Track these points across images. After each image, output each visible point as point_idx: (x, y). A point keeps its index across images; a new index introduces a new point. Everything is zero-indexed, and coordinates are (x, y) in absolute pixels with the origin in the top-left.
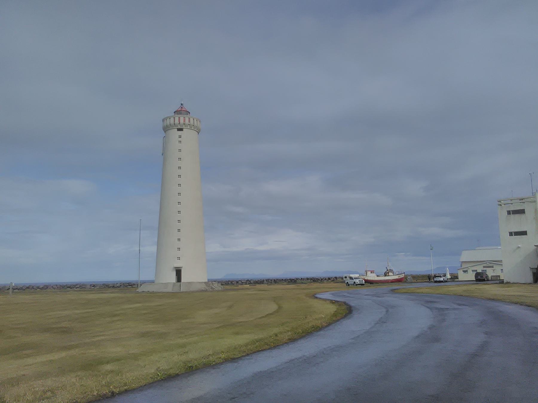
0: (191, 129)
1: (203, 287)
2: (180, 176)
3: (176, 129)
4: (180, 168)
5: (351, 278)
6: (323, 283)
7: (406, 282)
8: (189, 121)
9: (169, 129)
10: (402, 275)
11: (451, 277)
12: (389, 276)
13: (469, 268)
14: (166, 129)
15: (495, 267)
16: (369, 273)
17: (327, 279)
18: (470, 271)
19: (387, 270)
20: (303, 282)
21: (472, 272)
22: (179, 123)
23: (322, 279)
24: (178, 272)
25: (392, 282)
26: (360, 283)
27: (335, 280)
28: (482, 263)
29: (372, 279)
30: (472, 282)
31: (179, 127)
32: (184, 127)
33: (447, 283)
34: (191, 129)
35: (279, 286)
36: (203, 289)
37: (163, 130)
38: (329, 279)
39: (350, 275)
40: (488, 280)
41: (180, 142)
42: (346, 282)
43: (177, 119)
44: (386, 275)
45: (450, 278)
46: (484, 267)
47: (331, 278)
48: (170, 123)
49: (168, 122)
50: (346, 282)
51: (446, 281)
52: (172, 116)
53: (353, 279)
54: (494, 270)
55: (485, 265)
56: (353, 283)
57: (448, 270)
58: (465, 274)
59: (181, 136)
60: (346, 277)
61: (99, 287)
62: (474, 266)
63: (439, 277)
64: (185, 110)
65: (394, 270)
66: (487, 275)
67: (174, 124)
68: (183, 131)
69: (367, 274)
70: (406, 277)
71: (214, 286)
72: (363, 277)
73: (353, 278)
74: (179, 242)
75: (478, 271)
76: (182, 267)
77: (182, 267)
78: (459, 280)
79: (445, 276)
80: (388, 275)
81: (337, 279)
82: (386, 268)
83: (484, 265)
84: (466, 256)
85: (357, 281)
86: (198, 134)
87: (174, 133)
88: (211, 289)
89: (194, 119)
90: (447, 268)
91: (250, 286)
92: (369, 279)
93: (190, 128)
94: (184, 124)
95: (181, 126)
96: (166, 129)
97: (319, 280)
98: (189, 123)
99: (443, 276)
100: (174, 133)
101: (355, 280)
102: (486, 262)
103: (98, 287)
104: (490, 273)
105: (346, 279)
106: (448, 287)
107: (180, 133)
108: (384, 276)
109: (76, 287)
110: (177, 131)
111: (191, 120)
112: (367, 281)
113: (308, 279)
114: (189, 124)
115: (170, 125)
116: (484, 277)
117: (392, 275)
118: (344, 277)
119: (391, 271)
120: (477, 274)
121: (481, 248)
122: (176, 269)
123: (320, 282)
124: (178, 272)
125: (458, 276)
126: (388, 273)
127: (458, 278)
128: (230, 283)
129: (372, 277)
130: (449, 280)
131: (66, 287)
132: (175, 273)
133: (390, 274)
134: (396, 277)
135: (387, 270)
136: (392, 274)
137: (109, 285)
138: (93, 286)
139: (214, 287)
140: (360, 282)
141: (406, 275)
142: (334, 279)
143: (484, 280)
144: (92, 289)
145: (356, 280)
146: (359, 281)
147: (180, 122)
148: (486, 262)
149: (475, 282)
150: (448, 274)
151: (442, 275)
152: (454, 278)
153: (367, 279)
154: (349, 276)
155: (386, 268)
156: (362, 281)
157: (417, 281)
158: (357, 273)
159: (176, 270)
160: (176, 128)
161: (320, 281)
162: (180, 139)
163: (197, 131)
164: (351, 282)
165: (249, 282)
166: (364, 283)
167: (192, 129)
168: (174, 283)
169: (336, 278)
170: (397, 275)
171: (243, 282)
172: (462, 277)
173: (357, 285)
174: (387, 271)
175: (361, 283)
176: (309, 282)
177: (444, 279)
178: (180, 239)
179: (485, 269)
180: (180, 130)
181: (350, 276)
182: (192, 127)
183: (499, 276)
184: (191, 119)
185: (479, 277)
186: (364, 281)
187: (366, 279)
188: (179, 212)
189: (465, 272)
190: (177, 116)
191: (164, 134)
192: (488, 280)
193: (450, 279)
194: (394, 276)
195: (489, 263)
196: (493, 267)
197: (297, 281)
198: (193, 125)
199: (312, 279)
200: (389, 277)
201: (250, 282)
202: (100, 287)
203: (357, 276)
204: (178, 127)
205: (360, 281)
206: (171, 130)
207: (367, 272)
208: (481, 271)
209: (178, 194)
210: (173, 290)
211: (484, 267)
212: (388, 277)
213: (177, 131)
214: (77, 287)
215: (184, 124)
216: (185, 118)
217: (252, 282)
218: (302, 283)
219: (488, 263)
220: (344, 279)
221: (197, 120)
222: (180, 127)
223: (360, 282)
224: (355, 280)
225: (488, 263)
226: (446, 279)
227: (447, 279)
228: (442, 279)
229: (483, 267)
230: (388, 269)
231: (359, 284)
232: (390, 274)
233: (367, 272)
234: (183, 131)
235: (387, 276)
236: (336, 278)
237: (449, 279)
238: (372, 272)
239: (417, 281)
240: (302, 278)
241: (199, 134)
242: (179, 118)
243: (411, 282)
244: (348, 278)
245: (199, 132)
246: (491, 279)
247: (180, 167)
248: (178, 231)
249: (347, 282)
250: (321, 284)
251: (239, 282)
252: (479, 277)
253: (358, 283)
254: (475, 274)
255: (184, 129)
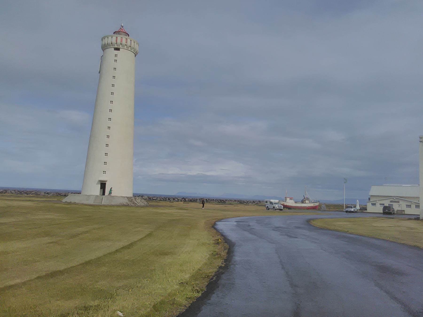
0: (128, 50)
1: (125, 201)
2: (112, 93)
3: (113, 48)
4: (113, 86)
5: (271, 203)
6: (248, 205)
7: (319, 210)
8: (126, 42)
9: (106, 48)
10: (317, 203)
11: (360, 208)
12: (305, 203)
13: (377, 202)
14: (104, 47)
15: (401, 202)
16: (288, 199)
17: (252, 202)
18: (378, 205)
19: (304, 198)
20: (231, 203)
21: (379, 205)
22: (116, 43)
23: (247, 202)
24: (103, 185)
25: (308, 209)
26: (278, 208)
27: (258, 203)
28: (388, 198)
29: (290, 205)
30: (378, 215)
31: (116, 47)
32: (121, 47)
33: (356, 214)
34: (128, 50)
35: (210, 205)
36: (125, 204)
37: (102, 48)
38: (254, 202)
39: (270, 200)
40: (394, 214)
41: (116, 61)
42: (267, 206)
43: (114, 38)
44: (303, 202)
45: (360, 209)
46: (391, 202)
47: (256, 201)
48: (107, 42)
49: (106, 41)
50: (267, 206)
51: (356, 212)
52: (110, 36)
53: (273, 204)
54: (400, 205)
55: (391, 200)
56: (273, 207)
57: (358, 202)
58: (373, 207)
59: (115, 56)
60: (266, 202)
61: (52, 195)
62: (382, 200)
63: (350, 208)
64: (125, 32)
65: (310, 199)
66: (393, 209)
67: (112, 43)
68: (119, 50)
69: (287, 200)
70: (320, 206)
71: (136, 202)
72: (282, 203)
73: (273, 202)
74: (106, 156)
75: (385, 205)
76: (107, 181)
77: (107, 181)
78: (368, 212)
79: (355, 207)
80: (304, 202)
81: (260, 202)
82: (304, 196)
83: (391, 200)
84: (375, 191)
85: (277, 206)
86: (135, 56)
87: (111, 52)
88: (133, 203)
89: (131, 40)
90: (358, 200)
91: (183, 203)
92: (288, 204)
93: (127, 49)
94: (121, 44)
95: (117, 46)
96: (104, 47)
97: (245, 202)
98: (126, 44)
99: (354, 207)
100: (111, 52)
101: (274, 205)
102: (393, 197)
103: (51, 195)
104: (396, 207)
105: (266, 203)
106: (373, 217)
107: (116, 52)
108: (301, 203)
109: (32, 193)
110: (114, 50)
111: (129, 41)
112: (285, 207)
113: (235, 201)
114: (126, 45)
115: (107, 44)
116: (391, 211)
117: (308, 203)
118: (265, 201)
119: (308, 199)
120: (385, 208)
121: (388, 185)
122: (101, 182)
123: (245, 204)
124: (103, 185)
125: (367, 207)
126: (305, 201)
127: (367, 210)
128: (167, 199)
129: (290, 203)
130: (358, 211)
131: (23, 193)
132: (99, 186)
133: (307, 201)
134: (312, 205)
135: (304, 198)
136: (309, 202)
137: (61, 194)
138: (47, 194)
139: (136, 203)
140: (279, 207)
141: (320, 204)
142: (258, 202)
143: (390, 214)
144: (46, 196)
145: (276, 205)
146: (278, 206)
147: (117, 42)
148: (393, 197)
149: (382, 215)
150: (358, 205)
151: (353, 206)
152: (363, 209)
153: (286, 205)
154: (270, 201)
155: (304, 196)
156: (281, 206)
157: (329, 209)
158: (276, 198)
159: (101, 183)
160: (113, 47)
161: (246, 203)
162: (116, 58)
163: (134, 53)
164: (271, 206)
165: (184, 200)
166: (282, 209)
167: (129, 50)
168: (97, 196)
169: (260, 202)
170: (312, 203)
171: (178, 200)
172: (370, 208)
173: (276, 209)
174: (304, 199)
175: (279, 208)
176: (236, 204)
177: (354, 210)
178: (107, 154)
179: (392, 203)
180: (117, 49)
181: (271, 201)
182: (130, 48)
183: (404, 211)
184: (128, 39)
185: (386, 210)
186: (282, 207)
187: (285, 204)
188: (109, 128)
189: (374, 204)
190: (114, 36)
191: (101, 53)
192: (394, 214)
193: (360, 210)
194: (310, 204)
195: (414, 202)
196: (398, 202)
197: (226, 202)
198: (130, 46)
199: (239, 201)
200: (305, 204)
201: (185, 199)
202: (53, 195)
203: (277, 201)
204: (114, 47)
205: (279, 206)
206: (109, 49)
207: (287, 198)
208: (388, 205)
209: (110, 110)
210: (94, 203)
211: (391, 202)
212: (304, 204)
213: (114, 50)
214: (33, 194)
215: (121, 44)
216: (127, 39)
217: (187, 199)
218: (230, 204)
219: (395, 198)
220: (265, 203)
221: (134, 42)
222: (117, 47)
223: (279, 207)
224: (274, 205)
225: (395, 198)
226: (356, 210)
227: (357, 210)
228: (352, 210)
229: (389, 202)
230: (305, 197)
231: (278, 209)
232: (307, 201)
233: (287, 198)
234: (119, 50)
235: (304, 203)
236: (260, 201)
237: (358, 210)
238: (291, 199)
239: (329, 209)
240: (230, 199)
241: (136, 56)
242: (117, 37)
243: (325, 211)
244: (268, 203)
245: (137, 55)
246: (397, 213)
247: (114, 85)
248: (106, 146)
249: (268, 207)
250: (246, 206)
251: (176, 199)
252: (386, 210)
253: (277, 208)
254: (383, 207)
255: (120, 49)
